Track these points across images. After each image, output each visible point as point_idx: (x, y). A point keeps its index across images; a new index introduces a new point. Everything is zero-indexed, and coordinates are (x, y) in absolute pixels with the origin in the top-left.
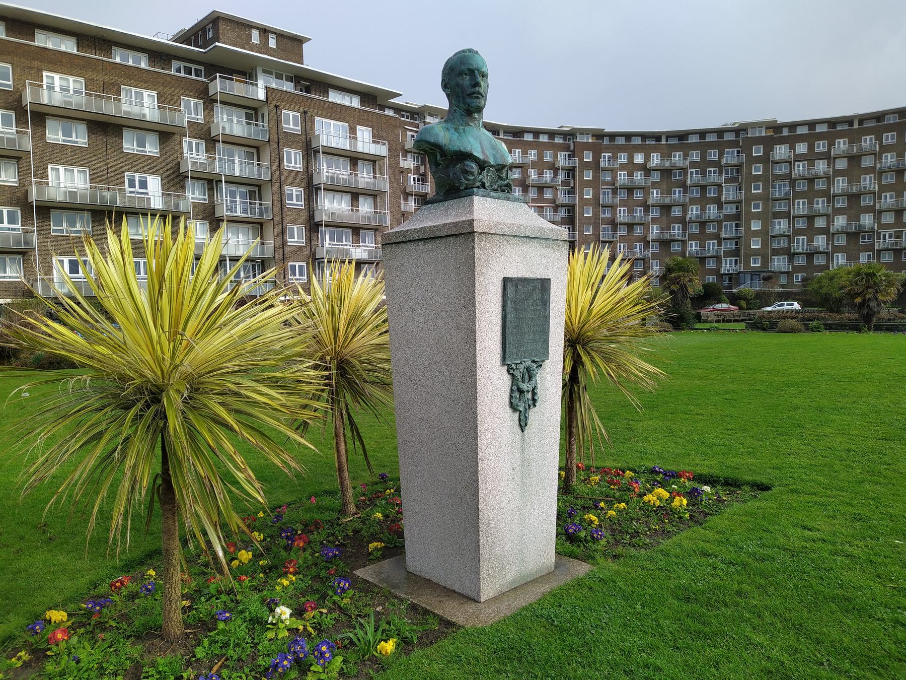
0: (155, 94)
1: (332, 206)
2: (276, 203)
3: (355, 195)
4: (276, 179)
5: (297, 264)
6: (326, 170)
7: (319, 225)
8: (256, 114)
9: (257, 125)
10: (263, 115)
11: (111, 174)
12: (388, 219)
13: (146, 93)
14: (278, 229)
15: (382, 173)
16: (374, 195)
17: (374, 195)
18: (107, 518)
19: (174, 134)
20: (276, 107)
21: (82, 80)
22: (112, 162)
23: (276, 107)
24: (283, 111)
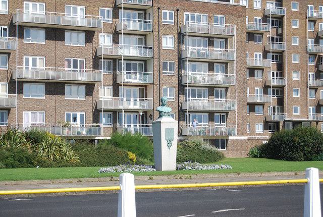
0: (84, 8)
1: (192, 75)
2: (155, 72)
3: (211, 66)
4: (156, 82)
5: (168, 12)
6: (191, 49)
7: (185, 111)
8: (145, 14)
9: (146, 22)
10: (149, 14)
11: (57, 59)
12: (235, 80)
13: (79, 8)
14: (156, 90)
15: (232, 47)
16: (225, 65)
17: (225, 65)
18: (48, 35)
19: (94, 32)
20: (159, 8)
21: (44, 4)
22: (58, 52)
23: (159, 8)
24: (163, 11)
